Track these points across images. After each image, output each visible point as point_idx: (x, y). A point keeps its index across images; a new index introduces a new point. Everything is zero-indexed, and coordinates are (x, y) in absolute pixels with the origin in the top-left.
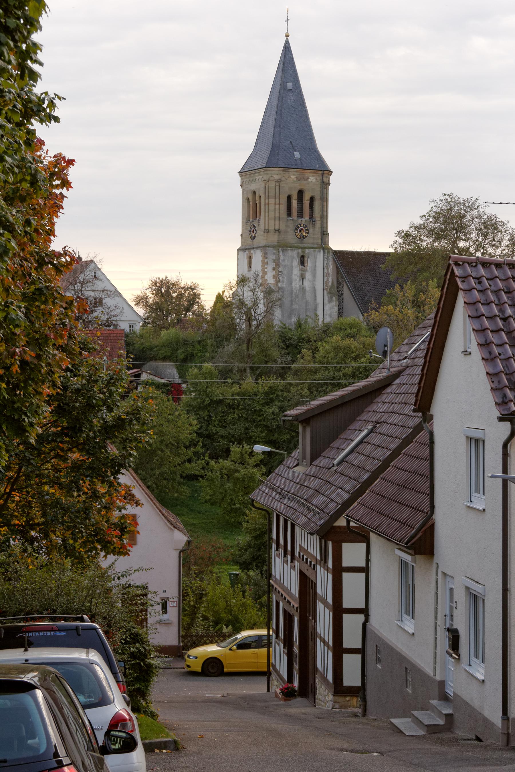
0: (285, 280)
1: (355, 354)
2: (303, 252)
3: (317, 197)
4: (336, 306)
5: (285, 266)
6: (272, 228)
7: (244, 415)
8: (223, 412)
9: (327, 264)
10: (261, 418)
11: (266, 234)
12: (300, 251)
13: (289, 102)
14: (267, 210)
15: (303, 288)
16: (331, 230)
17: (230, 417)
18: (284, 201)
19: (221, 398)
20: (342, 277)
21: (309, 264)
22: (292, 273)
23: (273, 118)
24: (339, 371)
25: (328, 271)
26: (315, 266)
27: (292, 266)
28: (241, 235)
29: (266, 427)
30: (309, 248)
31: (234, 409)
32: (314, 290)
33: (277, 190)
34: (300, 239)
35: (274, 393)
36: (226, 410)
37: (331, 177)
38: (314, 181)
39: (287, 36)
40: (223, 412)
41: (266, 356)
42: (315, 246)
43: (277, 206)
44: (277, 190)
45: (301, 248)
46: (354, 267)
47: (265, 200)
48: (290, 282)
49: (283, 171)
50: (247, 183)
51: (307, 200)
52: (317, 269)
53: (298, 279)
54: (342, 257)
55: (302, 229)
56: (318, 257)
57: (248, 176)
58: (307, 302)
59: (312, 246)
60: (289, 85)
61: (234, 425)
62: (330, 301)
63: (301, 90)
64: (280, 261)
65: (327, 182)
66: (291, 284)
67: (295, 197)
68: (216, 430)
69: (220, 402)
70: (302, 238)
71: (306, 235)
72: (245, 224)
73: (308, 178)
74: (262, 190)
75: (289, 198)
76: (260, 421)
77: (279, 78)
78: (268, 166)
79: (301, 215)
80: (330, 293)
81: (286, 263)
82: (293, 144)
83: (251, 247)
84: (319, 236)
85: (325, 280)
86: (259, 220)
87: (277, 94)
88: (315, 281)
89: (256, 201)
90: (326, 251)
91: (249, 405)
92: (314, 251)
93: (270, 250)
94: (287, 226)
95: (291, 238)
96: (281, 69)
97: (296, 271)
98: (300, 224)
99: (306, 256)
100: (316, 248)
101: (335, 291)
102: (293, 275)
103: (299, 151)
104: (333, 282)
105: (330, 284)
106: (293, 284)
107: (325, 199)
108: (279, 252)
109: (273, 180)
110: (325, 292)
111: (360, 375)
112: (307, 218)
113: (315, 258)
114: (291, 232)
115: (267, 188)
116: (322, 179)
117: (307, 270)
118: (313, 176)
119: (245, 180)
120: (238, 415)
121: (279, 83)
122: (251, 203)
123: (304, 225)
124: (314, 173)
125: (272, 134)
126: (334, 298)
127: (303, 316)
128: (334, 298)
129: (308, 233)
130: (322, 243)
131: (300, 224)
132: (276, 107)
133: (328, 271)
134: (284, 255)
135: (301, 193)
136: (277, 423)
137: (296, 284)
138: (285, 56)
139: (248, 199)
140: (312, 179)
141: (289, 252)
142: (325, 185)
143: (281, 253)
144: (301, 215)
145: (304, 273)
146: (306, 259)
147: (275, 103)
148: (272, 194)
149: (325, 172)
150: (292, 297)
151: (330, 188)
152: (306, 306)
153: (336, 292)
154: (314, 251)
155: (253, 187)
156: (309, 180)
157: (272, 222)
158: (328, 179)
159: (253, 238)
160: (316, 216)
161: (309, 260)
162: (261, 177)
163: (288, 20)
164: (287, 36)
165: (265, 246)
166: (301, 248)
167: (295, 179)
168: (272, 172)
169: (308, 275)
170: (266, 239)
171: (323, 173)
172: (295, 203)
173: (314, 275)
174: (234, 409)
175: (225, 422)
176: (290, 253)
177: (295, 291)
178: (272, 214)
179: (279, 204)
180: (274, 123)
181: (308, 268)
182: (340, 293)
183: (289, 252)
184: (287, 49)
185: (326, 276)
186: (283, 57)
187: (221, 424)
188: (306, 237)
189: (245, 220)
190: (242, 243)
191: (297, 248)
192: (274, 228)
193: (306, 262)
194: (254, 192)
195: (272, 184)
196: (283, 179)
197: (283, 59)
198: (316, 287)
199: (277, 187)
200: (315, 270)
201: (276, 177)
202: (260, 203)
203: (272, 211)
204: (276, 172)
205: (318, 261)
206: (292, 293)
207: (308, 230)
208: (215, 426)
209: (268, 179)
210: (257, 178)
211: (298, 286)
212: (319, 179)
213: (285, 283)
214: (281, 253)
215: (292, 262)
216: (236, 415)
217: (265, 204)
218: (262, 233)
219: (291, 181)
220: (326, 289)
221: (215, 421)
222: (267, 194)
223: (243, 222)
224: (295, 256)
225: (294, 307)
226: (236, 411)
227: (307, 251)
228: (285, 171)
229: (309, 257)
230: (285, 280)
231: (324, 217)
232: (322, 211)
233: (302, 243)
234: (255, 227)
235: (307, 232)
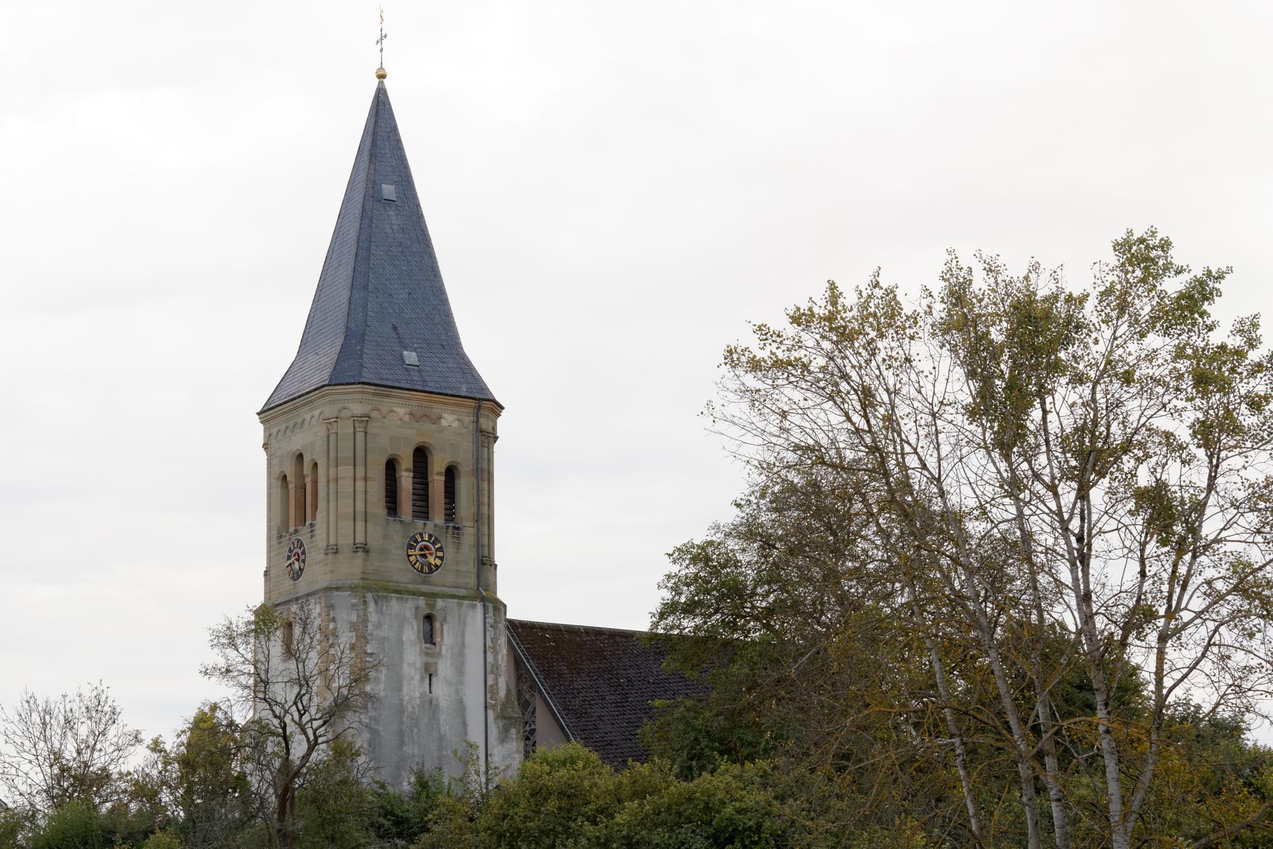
0: (383, 679)
1: (592, 806)
2: (432, 606)
3: (465, 469)
4: (518, 752)
5: (383, 640)
6: (346, 541)
9: (494, 640)
11: (330, 557)
12: (422, 602)
14: (332, 496)
16: (501, 555)
18: (378, 473)
20: (533, 687)
21: (447, 637)
22: (401, 659)
23: (346, 272)
25: (496, 659)
26: (463, 645)
27: (400, 642)
28: (266, 574)
30: (444, 596)
32: (461, 708)
33: (360, 444)
34: (421, 571)
37: (499, 420)
38: (455, 424)
39: (382, 77)
42: (462, 592)
44: (360, 444)
46: (559, 662)
47: (328, 469)
48: (397, 685)
49: (374, 394)
50: (280, 437)
51: (439, 474)
52: (466, 651)
53: (417, 677)
54: (525, 633)
55: (426, 548)
56: (469, 620)
57: (282, 418)
58: (441, 738)
60: (388, 190)
62: (503, 739)
63: (418, 206)
64: (370, 627)
65: (490, 430)
66: (400, 689)
67: (406, 462)
70: (426, 569)
71: (438, 562)
72: (275, 542)
74: (320, 445)
75: (391, 465)
77: (362, 176)
78: (337, 380)
79: (423, 511)
80: (502, 716)
81: (386, 631)
82: (400, 331)
83: (292, 596)
84: (471, 567)
85: (490, 682)
86: (312, 525)
88: (461, 683)
89: (303, 477)
92: (460, 605)
94: (386, 537)
95: (397, 568)
96: (366, 153)
97: (413, 656)
98: (421, 535)
99: (439, 616)
100: (463, 598)
101: (516, 712)
102: (405, 666)
103: (415, 350)
104: (508, 691)
106: (405, 689)
107: (484, 474)
108: (365, 602)
109: (348, 418)
110: (490, 713)
112: (438, 518)
113: (462, 622)
114: (397, 551)
115: (332, 437)
117: (439, 655)
118: (453, 412)
119: (274, 431)
121: (361, 186)
122: (292, 486)
123: (430, 536)
124: (456, 405)
125: (345, 307)
126: (513, 731)
127: (429, 767)
128: (513, 731)
129: (441, 558)
130: (478, 585)
131: (421, 535)
133: (496, 659)
134: (380, 612)
135: (421, 455)
137: (413, 688)
138: (376, 122)
139: (285, 477)
140: (452, 420)
141: (394, 603)
143: (372, 607)
144: (423, 511)
146: (437, 625)
147: (353, 235)
148: (346, 453)
149: (485, 407)
150: (401, 723)
151: (497, 447)
152: (440, 748)
153: (518, 714)
154: (460, 605)
155: (297, 442)
156: (444, 423)
157: (347, 526)
158: (491, 424)
159: (296, 575)
161: (445, 628)
162: (316, 413)
163: (383, 37)
164: (382, 77)
165: (329, 589)
167: (407, 418)
168: (347, 397)
169: (445, 668)
170: (332, 571)
171: (479, 407)
172: (406, 480)
173: (460, 668)
176: (395, 605)
177: (410, 709)
178: (346, 505)
179: (366, 479)
180: (350, 281)
181: (444, 648)
182: (527, 728)
183: (394, 603)
184: (381, 108)
186: (372, 125)
188: (437, 567)
189: (275, 533)
190: (268, 592)
191: (414, 593)
193: (438, 632)
195: (346, 429)
196: (374, 414)
197: (371, 129)
198: (466, 699)
199: (360, 436)
201: (358, 409)
202: (315, 483)
203: (349, 501)
204: (358, 396)
205: (467, 631)
207: (440, 549)
211: (417, 695)
212: (468, 419)
213: (382, 686)
214: (372, 607)
215: (401, 632)
218: (321, 557)
219: (397, 425)
220: (493, 707)
222: (332, 455)
224: (409, 614)
225: (409, 749)
227: (440, 603)
228: (379, 395)
230: (383, 679)
231: (484, 519)
232: (479, 504)
233: (425, 583)
234: (302, 545)
235: (440, 554)
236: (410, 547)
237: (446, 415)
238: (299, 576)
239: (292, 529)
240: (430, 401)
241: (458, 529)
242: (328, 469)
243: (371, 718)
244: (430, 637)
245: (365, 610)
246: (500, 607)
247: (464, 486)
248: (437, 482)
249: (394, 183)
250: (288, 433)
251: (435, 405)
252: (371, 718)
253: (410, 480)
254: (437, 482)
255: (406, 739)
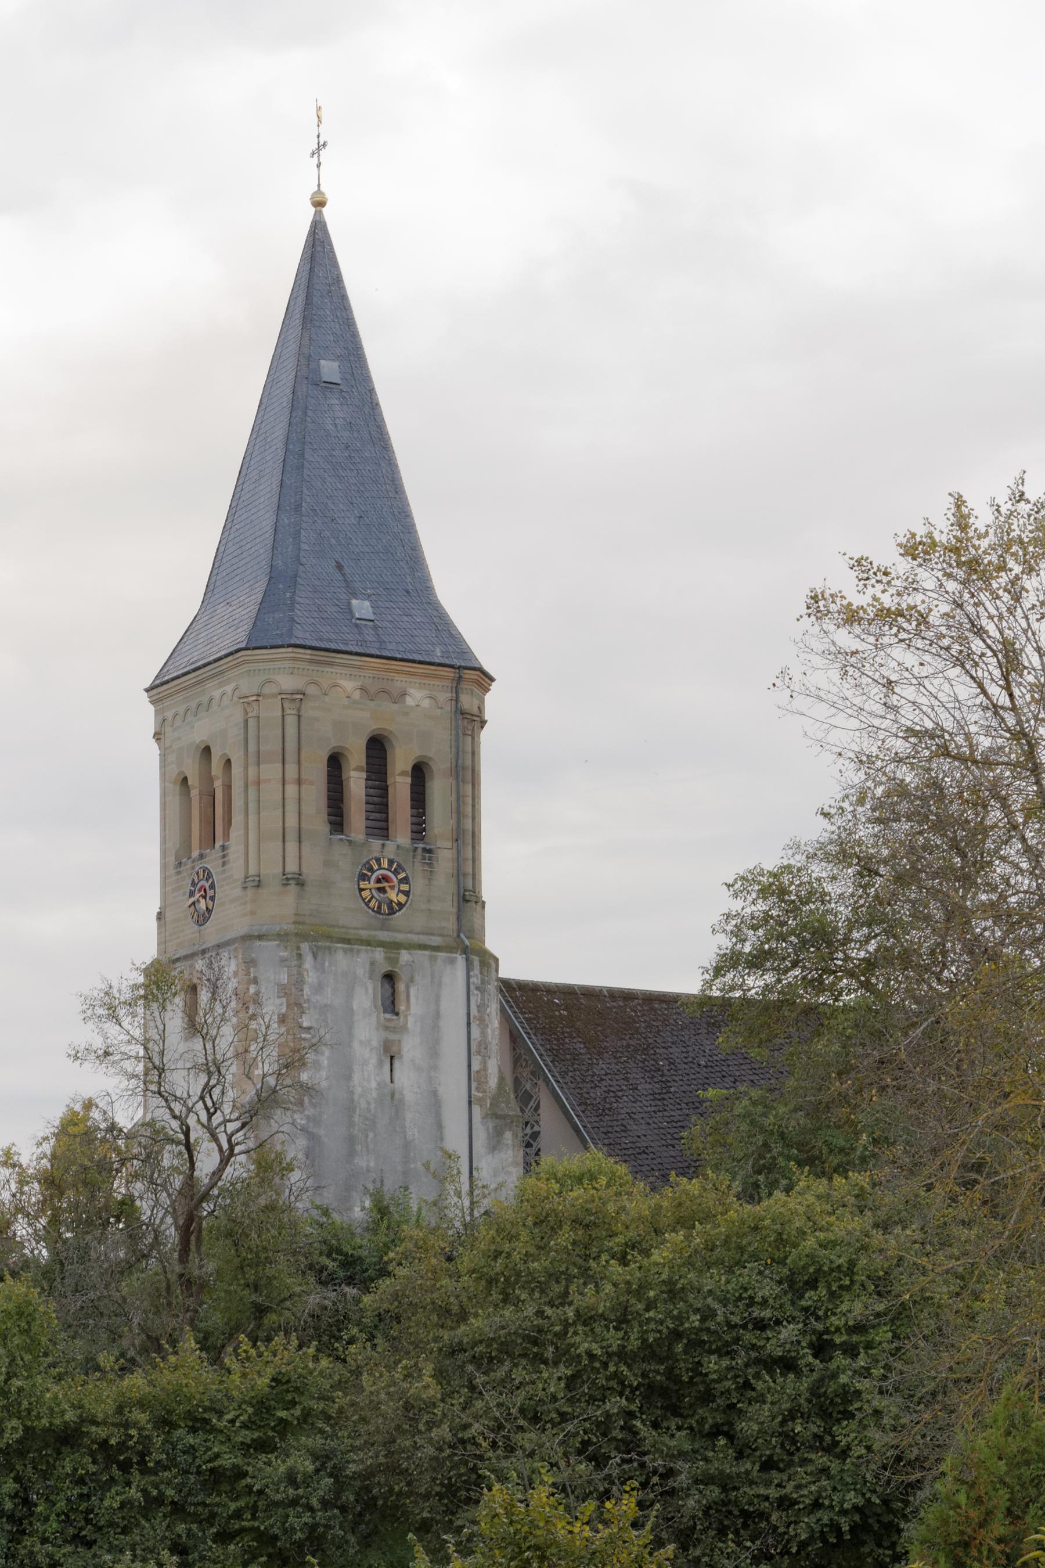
4: (515, 1164)
5: (324, 1009)
6: (272, 870)
7: (170, 1492)
8: (81, 1481)
9: (482, 1007)
10: (241, 1503)
11: (250, 892)
12: (379, 954)
13: (330, 427)
14: (252, 806)
15: (393, 1095)
17: (112, 1500)
18: (317, 773)
19: (70, 1416)
20: (537, 1072)
21: (415, 1004)
22: (351, 1035)
24: (562, 1304)
25: (483, 1034)
26: (438, 1015)
27: (350, 1012)
28: (160, 916)
29: (266, 1539)
30: (410, 946)
31: (125, 1467)
32: (435, 1103)
34: (379, 912)
35: (294, 1403)
36: (92, 1468)
37: (488, 697)
38: (426, 703)
39: (319, 203)
40: (81, 1481)
41: (256, 1288)
42: (436, 941)
43: (291, 790)
45: (382, 944)
46: (575, 1043)
47: (246, 768)
49: (311, 662)
50: (178, 721)
51: (403, 773)
53: (374, 1061)
54: (527, 1001)
55: (386, 879)
58: (407, 1146)
59: (423, 939)
60: (330, 369)
61: (125, 1531)
62: (495, 1145)
63: (372, 391)
64: (307, 990)
65: (475, 711)
66: (349, 1078)
68: (50, 1556)
69: (67, 1438)
70: (385, 908)
71: (402, 898)
72: (172, 871)
73: (404, 694)
76: (238, 1515)
77: (292, 347)
78: (257, 642)
79: (380, 825)
82: (347, 570)
84: (449, 906)
85: (475, 1067)
87: (286, 401)
88: (435, 1068)
90: (476, 960)
91: (191, 1450)
93: (269, 951)
95: (345, 908)
97: (367, 1031)
98: (378, 860)
99: (403, 975)
100: (437, 949)
101: (512, 1108)
102: (356, 1045)
103: (368, 597)
104: (501, 1079)
105: (493, 1082)
106: (356, 1078)
107: (466, 774)
108: (300, 956)
109: (274, 696)
110: (476, 1110)
111: (652, 1314)
112: (402, 836)
114: (346, 885)
115: (252, 723)
116: (457, 700)
117: (404, 1029)
119: (169, 714)
120: (144, 1492)
123: (391, 862)
125: (269, 536)
126: (508, 1135)
128: (508, 1135)
129: (407, 894)
130: (459, 931)
131: (378, 860)
132: (280, 445)
133: (483, 1034)
135: (377, 747)
136: (307, 1518)
137: (368, 1077)
139: (185, 780)
141: (340, 956)
142: (469, 722)
143: (308, 962)
144: (380, 827)
145: (393, 1037)
146: (401, 987)
147: (279, 432)
148: (271, 745)
150: (351, 1124)
151: (485, 736)
155: (200, 732)
156: (409, 701)
158: (476, 702)
159: (203, 919)
160: (436, 831)
161: (413, 991)
162: (229, 688)
163: (321, 146)
164: (319, 203)
165: (247, 938)
166: (382, 944)
167: (357, 695)
168: (271, 665)
169: (411, 1047)
170: (253, 913)
172: (356, 783)
173: (434, 1051)
174: (125, 1467)
175: (88, 1521)
176: (341, 960)
178: (272, 820)
179: (299, 782)
180: (275, 500)
182: (528, 1131)
183: (340, 956)
184: (318, 248)
185: (479, 1052)
186: (306, 274)
187: (71, 1531)
188: (401, 905)
189: (171, 859)
190: (163, 943)
191: (368, 943)
192: (281, 870)
194: (207, 751)
195: (271, 711)
196: (311, 690)
198: (441, 1090)
199: (291, 721)
200: (435, 1027)
201: (287, 682)
202: (228, 787)
203: (276, 806)
204: (287, 664)
205: (443, 996)
206: (350, 1108)
207: (405, 880)
208: (44, 1541)
209: (255, 691)
210: (217, 694)
211: (374, 1085)
212: (444, 696)
213: (324, 1074)
214: (308, 962)
215: (350, 995)
216: (133, 1493)
217: (246, 786)
218: (238, 892)
219: (343, 705)
220: (481, 1101)
221: (47, 1519)
222: (252, 748)
223: (164, 867)
224: (361, 971)
225: (360, 1162)
226: (136, 1476)
227: (405, 956)
229: (412, 980)
231: (466, 838)
233: (384, 927)
234: (209, 876)
235: (405, 887)
236: (363, 877)
237: (412, 691)
238: (206, 920)
239: (195, 854)
240: (387, 670)
241: (430, 851)
242: (246, 768)
243: (308, 1118)
244: (391, 1005)
245: (300, 966)
246: (488, 961)
247: (438, 790)
248: (400, 786)
249: (338, 358)
250: (190, 718)
251: (397, 677)
252: (308, 1118)
253: (363, 783)
254: (400, 786)
255: (359, 1148)
